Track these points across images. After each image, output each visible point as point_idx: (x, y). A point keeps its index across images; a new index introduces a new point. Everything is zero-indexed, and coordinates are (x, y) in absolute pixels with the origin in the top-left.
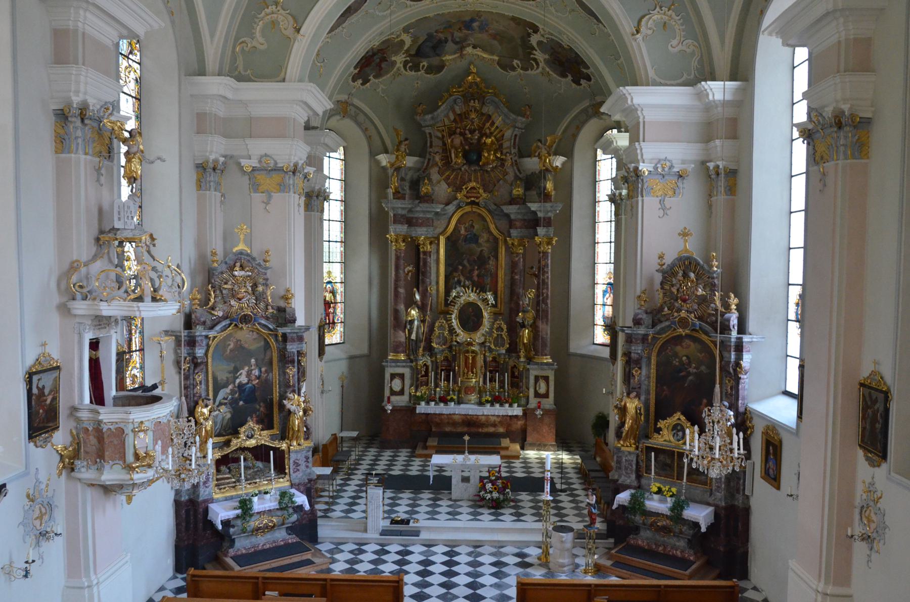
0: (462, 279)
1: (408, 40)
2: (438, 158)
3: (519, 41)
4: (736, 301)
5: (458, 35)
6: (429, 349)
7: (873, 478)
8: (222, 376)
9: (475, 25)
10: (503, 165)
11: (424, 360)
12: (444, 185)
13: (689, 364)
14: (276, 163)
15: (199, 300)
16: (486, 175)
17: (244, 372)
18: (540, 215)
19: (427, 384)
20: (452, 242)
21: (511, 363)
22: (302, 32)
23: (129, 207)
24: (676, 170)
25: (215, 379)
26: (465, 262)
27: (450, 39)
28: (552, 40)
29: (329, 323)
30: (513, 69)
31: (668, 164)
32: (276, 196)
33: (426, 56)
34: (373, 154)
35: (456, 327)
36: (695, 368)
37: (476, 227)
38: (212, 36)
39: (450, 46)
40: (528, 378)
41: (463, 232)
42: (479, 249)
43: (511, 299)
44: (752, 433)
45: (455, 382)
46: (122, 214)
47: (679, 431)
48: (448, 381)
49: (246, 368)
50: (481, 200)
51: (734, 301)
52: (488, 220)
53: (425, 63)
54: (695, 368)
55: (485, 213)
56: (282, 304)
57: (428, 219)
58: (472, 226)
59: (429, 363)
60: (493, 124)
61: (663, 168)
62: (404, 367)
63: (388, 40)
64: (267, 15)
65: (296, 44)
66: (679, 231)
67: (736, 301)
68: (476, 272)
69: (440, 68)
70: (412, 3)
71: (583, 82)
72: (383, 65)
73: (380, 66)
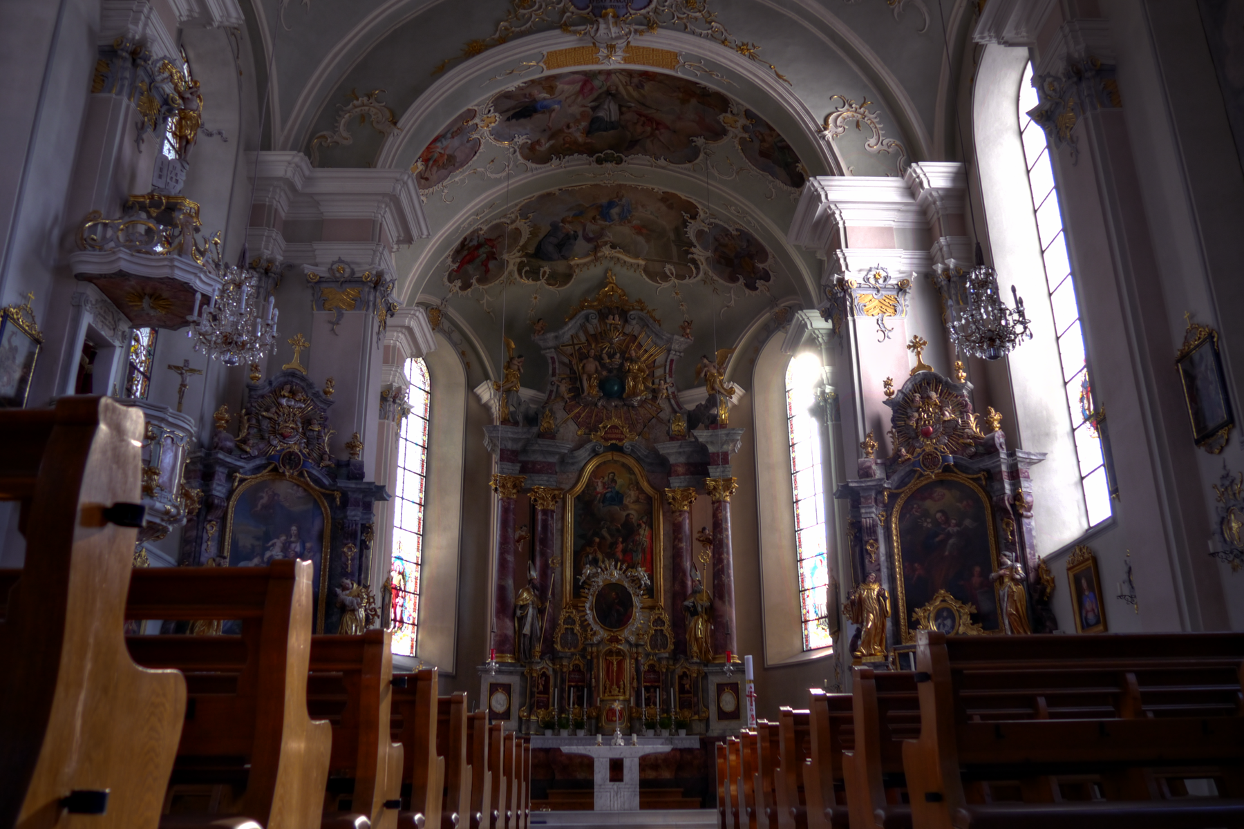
0: (600, 556)
1: (524, 227)
2: (563, 388)
3: (672, 236)
4: (997, 417)
5: (591, 227)
6: (550, 652)
7: (1225, 467)
8: (246, 542)
9: (615, 211)
10: (655, 398)
11: (542, 666)
12: (572, 427)
13: (947, 521)
14: (353, 272)
15: (227, 421)
16: (633, 413)
17: (279, 542)
18: (711, 449)
19: (547, 707)
20: (585, 504)
21: (679, 670)
22: (400, 125)
23: (174, 168)
24: (893, 282)
25: (234, 543)
26: (604, 532)
27: (580, 233)
28: (716, 225)
29: (395, 620)
30: (665, 278)
31: (883, 274)
32: (349, 314)
33: (549, 259)
34: (471, 386)
35: (591, 621)
36: (956, 525)
37: (619, 481)
38: (283, 129)
39: (581, 245)
40: (705, 691)
41: (600, 489)
42: (625, 514)
43: (674, 578)
44: (1054, 589)
45: (590, 704)
46: (165, 171)
47: (945, 619)
48: (581, 704)
49: (283, 538)
50: (626, 444)
51: (996, 417)
52: (636, 470)
53: (547, 269)
54: (956, 525)
55: (631, 462)
56: (344, 457)
57: (550, 464)
58: (614, 481)
59: (550, 673)
60: (640, 346)
61: (876, 280)
62: (511, 673)
63: (497, 226)
64: (355, 107)
65: (391, 139)
66: (908, 343)
67: (997, 417)
68: (620, 547)
69: (568, 277)
70: (534, 165)
71: (759, 283)
72: (491, 265)
73: (486, 266)
